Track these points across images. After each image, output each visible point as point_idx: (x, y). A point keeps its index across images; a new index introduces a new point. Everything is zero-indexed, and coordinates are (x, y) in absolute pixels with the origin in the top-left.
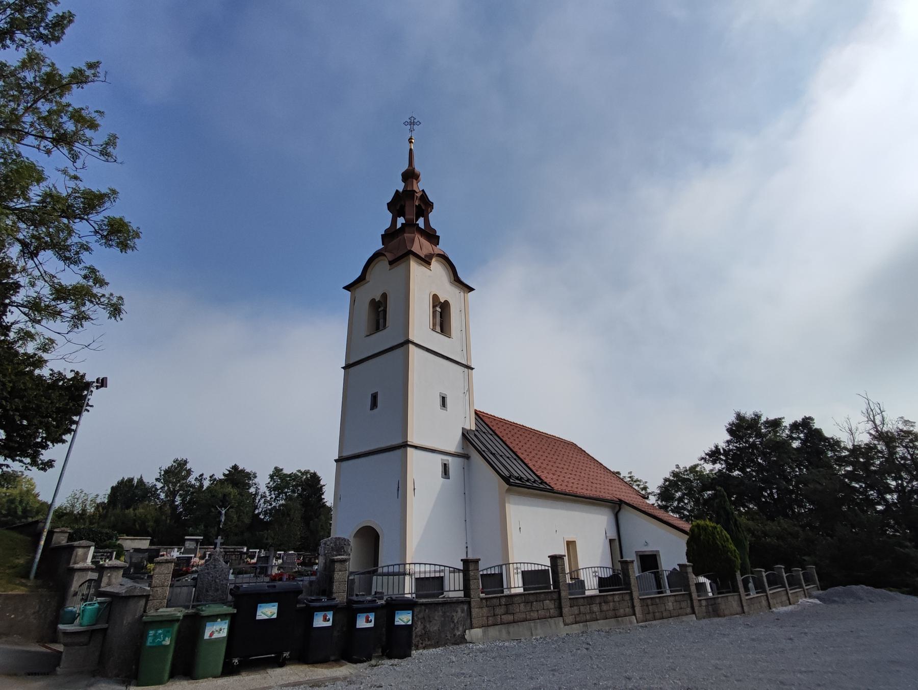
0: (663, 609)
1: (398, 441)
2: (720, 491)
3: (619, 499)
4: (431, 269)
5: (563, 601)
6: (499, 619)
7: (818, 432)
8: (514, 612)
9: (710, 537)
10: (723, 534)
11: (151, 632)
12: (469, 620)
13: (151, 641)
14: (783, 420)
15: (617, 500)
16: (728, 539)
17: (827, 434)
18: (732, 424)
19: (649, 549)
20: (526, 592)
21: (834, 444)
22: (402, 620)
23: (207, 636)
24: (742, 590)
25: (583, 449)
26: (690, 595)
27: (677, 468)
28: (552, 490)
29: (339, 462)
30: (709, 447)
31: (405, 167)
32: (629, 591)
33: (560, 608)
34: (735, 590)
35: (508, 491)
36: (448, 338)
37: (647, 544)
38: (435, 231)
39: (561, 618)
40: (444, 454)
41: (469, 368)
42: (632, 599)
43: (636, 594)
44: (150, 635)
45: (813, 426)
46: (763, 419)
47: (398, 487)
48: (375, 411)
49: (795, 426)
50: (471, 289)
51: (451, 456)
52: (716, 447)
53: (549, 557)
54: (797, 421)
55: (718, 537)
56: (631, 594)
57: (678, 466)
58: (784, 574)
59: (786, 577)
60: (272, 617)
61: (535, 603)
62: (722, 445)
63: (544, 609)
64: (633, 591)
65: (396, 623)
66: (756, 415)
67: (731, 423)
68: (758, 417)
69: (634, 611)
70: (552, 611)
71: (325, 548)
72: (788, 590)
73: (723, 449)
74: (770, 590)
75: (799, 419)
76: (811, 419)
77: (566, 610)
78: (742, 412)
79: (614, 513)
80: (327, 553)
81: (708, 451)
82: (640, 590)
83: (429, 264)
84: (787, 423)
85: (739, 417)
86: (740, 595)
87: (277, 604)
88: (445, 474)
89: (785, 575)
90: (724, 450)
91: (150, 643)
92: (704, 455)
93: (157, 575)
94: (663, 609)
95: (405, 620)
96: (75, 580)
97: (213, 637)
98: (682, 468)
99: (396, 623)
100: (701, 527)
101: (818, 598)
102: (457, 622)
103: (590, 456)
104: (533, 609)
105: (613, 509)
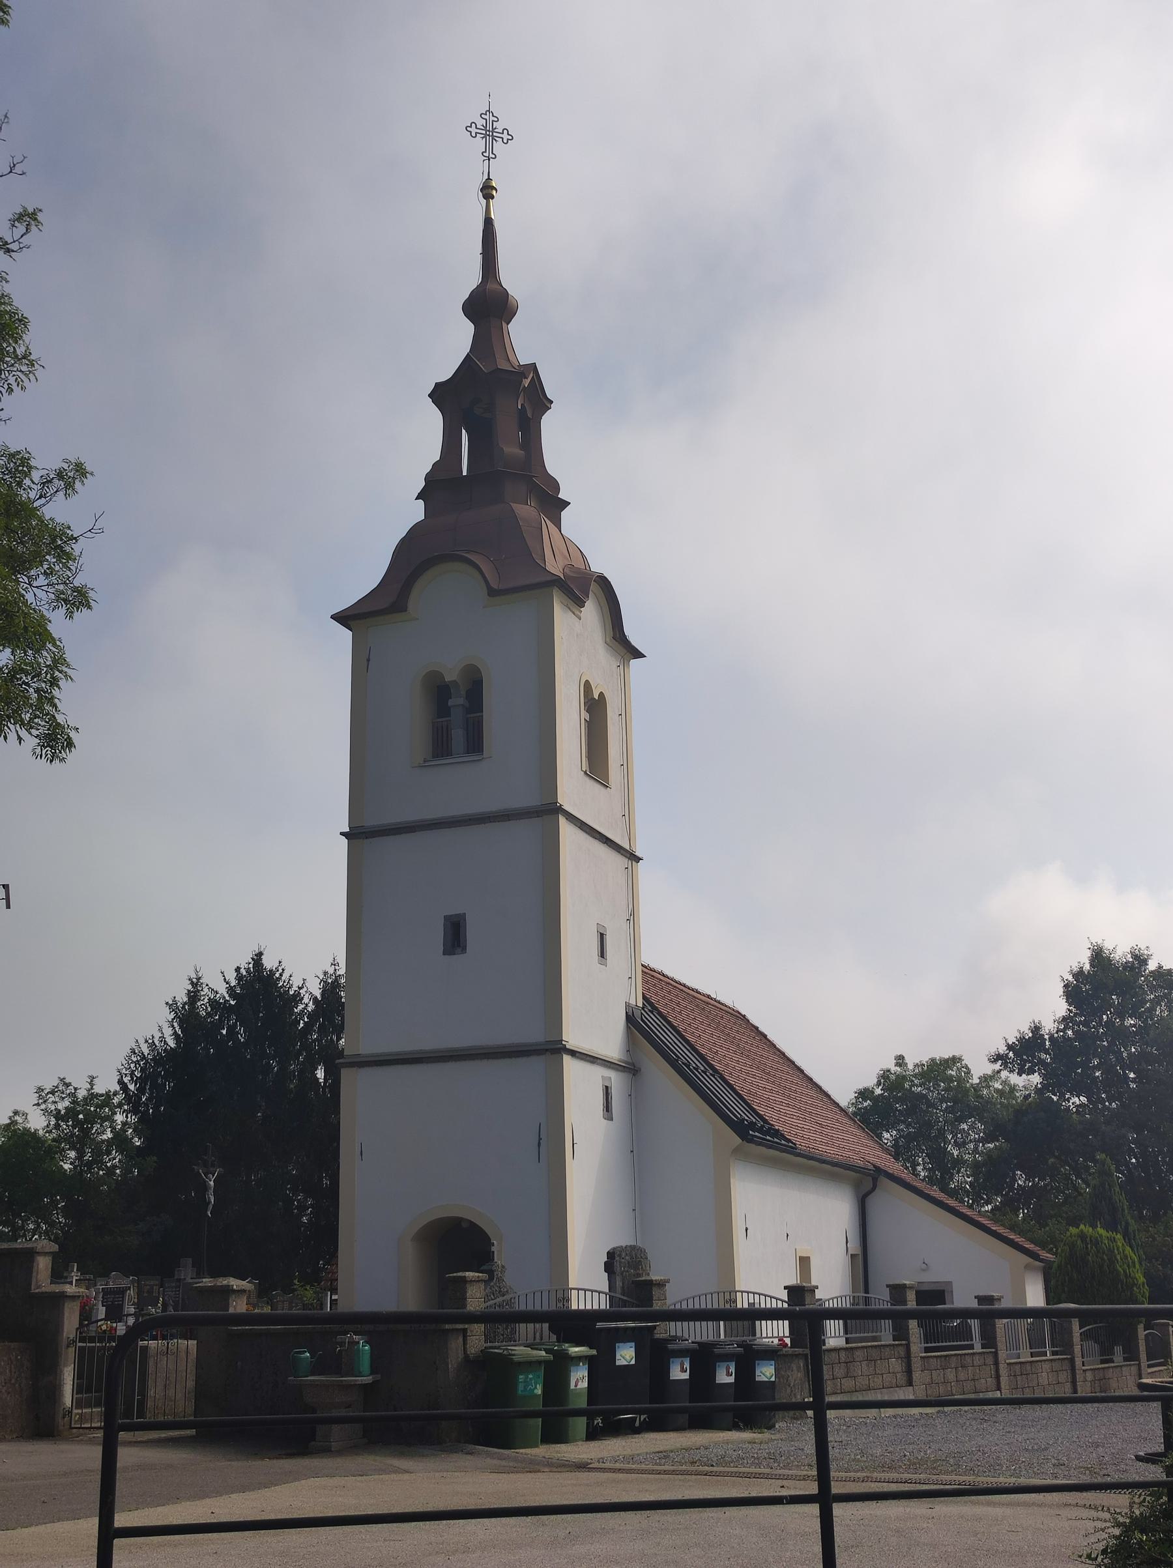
0: (1035, 1383)
1: (534, 1035)
2: (1103, 1163)
3: (874, 1166)
4: (582, 615)
5: (913, 1360)
6: (839, 1384)
8: (855, 1375)
9: (1105, 1257)
10: (1127, 1252)
11: (521, 1377)
12: (807, 1383)
13: (522, 1389)
15: (871, 1167)
16: (1134, 1262)
18: (1079, 975)
20: (848, 1345)
22: (764, 1375)
23: (572, 1386)
25: (762, 1029)
26: (1072, 1361)
27: (898, 1064)
28: (791, 1149)
30: (1015, 1027)
31: (472, 278)
32: (993, 1350)
33: (909, 1371)
35: (736, 1151)
36: (602, 789)
37: (926, 1267)
38: (556, 486)
39: (911, 1387)
40: (588, 1061)
41: (634, 858)
42: (996, 1363)
43: (1002, 1355)
44: (520, 1380)
46: (1152, 966)
47: (540, 1139)
48: (456, 959)
50: (638, 654)
51: (613, 1068)
52: (1036, 1029)
53: (785, 1288)
55: (1118, 1257)
56: (996, 1354)
60: (631, 1363)
61: (879, 1362)
62: (1049, 1026)
63: (889, 1373)
64: (999, 1349)
67: (1076, 969)
68: (1140, 960)
70: (899, 1376)
71: (620, 1262)
73: (1051, 1038)
74: (1149, 1366)
77: (916, 1376)
78: (1108, 945)
80: (624, 1271)
81: (1014, 1040)
82: (1008, 1349)
83: (581, 604)
85: (1099, 957)
86: (1139, 1365)
87: (633, 1344)
88: (607, 1111)
90: (1051, 1038)
91: (522, 1391)
92: (1003, 1049)
93: (470, 1300)
94: (1035, 1383)
95: (768, 1374)
96: (65, 1317)
97: (578, 1387)
98: (910, 1067)
100: (1088, 1239)
102: (794, 1386)
104: (878, 1372)
105: (857, 1186)
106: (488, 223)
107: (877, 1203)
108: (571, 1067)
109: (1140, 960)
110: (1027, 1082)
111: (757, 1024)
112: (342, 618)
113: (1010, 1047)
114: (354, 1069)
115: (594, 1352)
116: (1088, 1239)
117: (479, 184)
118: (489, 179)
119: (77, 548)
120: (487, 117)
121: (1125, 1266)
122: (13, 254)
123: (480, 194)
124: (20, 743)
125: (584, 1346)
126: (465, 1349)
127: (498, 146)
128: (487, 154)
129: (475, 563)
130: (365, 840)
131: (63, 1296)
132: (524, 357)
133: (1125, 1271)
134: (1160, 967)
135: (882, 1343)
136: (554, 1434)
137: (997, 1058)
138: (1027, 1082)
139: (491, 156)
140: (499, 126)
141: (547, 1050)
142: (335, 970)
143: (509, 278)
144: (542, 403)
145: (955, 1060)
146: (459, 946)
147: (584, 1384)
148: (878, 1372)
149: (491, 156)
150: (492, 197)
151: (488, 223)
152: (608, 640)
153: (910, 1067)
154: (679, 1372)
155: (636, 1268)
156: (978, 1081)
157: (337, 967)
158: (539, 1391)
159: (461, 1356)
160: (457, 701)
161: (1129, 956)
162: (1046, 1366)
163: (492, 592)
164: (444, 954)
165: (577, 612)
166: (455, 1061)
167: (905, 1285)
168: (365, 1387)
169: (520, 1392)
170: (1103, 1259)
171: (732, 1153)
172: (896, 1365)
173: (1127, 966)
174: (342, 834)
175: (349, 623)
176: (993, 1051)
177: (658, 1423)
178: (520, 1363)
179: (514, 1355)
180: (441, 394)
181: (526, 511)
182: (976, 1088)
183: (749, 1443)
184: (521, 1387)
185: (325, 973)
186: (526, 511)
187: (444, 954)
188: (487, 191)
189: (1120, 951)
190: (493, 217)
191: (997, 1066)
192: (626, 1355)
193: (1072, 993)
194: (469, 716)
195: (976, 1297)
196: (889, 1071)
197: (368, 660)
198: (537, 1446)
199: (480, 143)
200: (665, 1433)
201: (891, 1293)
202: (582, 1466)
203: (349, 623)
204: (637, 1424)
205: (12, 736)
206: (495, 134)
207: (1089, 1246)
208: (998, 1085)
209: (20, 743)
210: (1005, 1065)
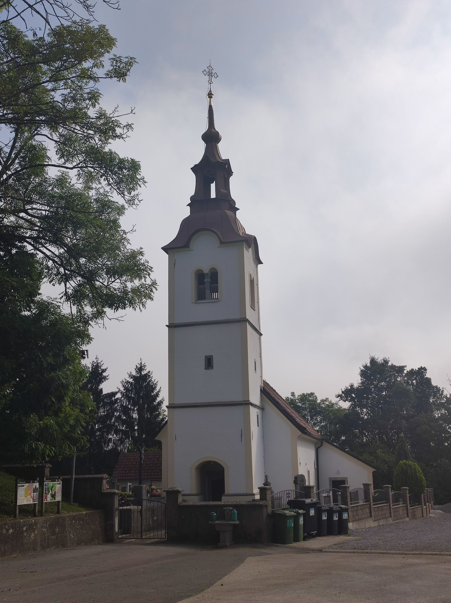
7: (429, 380)
14: (405, 368)
17: (434, 383)
19: (342, 475)
21: (437, 391)
24: (423, 504)
26: (407, 506)
29: (169, 408)
30: (344, 385)
31: (204, 128)
33: (371, 512)
34: (420, 504)
35: (299, 438)
36: (253, 310)
37: (338, 473)
38: (234, 203)
41: (261, 335)
42: (390, 508)
45: (425, 375)
46: (390, 364)
47: (242, 434)
48: (209, 371)
49: (412, 372)
54: (413, 369)
57: (293, 394)
58: (408, 494)
59: (409, 496)
62: (356, 385)
65: (343, 518)
66: (384, 361)
67: (364, 365)
69: (391, 515)
70: (368, 514)
72: (372, 505)
74: (374, 505)
75: (416, 368)
76: (425, 369)
77: (373, 514)
78: (376, 357)
79: (315, 448)
84: (408, 369)
89: (408, 495)
92: (341, 393)
98: (296, 396)
99: (343, 518)
100: (407, 465)
101: (440, 509)
103: (279, 395)
105: (316, 444)
106: (210, 108)
107: (321, 450)
108: (252, 409)
109: (386, 362)
110: (346, 405)
111: (272, 387)
112: (165, 249)
113: (343, 392)
114: (173, 409)
115: (305, 512)
116: (407, 465)
117: (207, 92)
118: (210, 91)
119: (128, 236)
120: (209, 68)
121: (420, 474)
122: (124, 139)
123: (207, 96)
124: (141, 312)
125: (301, 510)
126: (267, 512)
127: (213, 79)
128: (209, 82)
129: (216, 232)
130: (175, 328)
131: (115, 493)
132: (224, 156)
133: (419, 476)
134: (392, 365)
135: (360, 504)
136: (296, 539)
137: (338, 396)
138: (346, 405)
139: (211, 82)
140: (214, 72)
141: (244, 404)
142: (97, 361)
143: (218, 127)
144: (230, 173)
145: (312, 394)
146: (210, 366)
147: (302, 523)
148: (364, 513)
149: (211, 82)
150: (212, 97)
151: (210, 108)
152: (254, 258)
153: (296, 396)
154: (324, 518)
155: (303, 482)
156: (320, 401)
157: (98, 360)
158: (293, 525)
159: (266, 514)
160: (207, 280)
161: (383, 361)
162: (401, 508)
163: (222, 243)
164: (205, 369)
165: (248, 250)
166: (210, 407)
167: (369, 484)
168: (235, 525)
169: (288, 526)
170: (413, 472)
171: (298, 437)
172: (367, 510)
173: (382, 365)
174: (166, 326)
175: (168, 250)
176: (337, 394)
177: (319, 534)
178: (288, 516)
179: (286, 514)
180: (195, 169)
181: (229, 213)
182: (319, 404)
183: (355, 540)
184: (288, 524)
185: (93, 362)
186: (229, 213)
187: (205, 369)
188: (210, 95)
189: (380, 360)
190: (212, 105)
191: (338, 399)
192: (312, 512)
193: (363, 374)
194: (211, 285)
195: (363, 484)
196: (288, 397)
197: (175, 264)
198: (292, 543)
199: (207, 78)
200: (320, 537)
201: (364, 487)
202: (320, 551)
203: (168, 250)
204: (314, 534)
205: (138, 309)
206: (212, 74)
207: (408, 467)
208: (327, 403)
209: (141, 312)
210: (341, 399)
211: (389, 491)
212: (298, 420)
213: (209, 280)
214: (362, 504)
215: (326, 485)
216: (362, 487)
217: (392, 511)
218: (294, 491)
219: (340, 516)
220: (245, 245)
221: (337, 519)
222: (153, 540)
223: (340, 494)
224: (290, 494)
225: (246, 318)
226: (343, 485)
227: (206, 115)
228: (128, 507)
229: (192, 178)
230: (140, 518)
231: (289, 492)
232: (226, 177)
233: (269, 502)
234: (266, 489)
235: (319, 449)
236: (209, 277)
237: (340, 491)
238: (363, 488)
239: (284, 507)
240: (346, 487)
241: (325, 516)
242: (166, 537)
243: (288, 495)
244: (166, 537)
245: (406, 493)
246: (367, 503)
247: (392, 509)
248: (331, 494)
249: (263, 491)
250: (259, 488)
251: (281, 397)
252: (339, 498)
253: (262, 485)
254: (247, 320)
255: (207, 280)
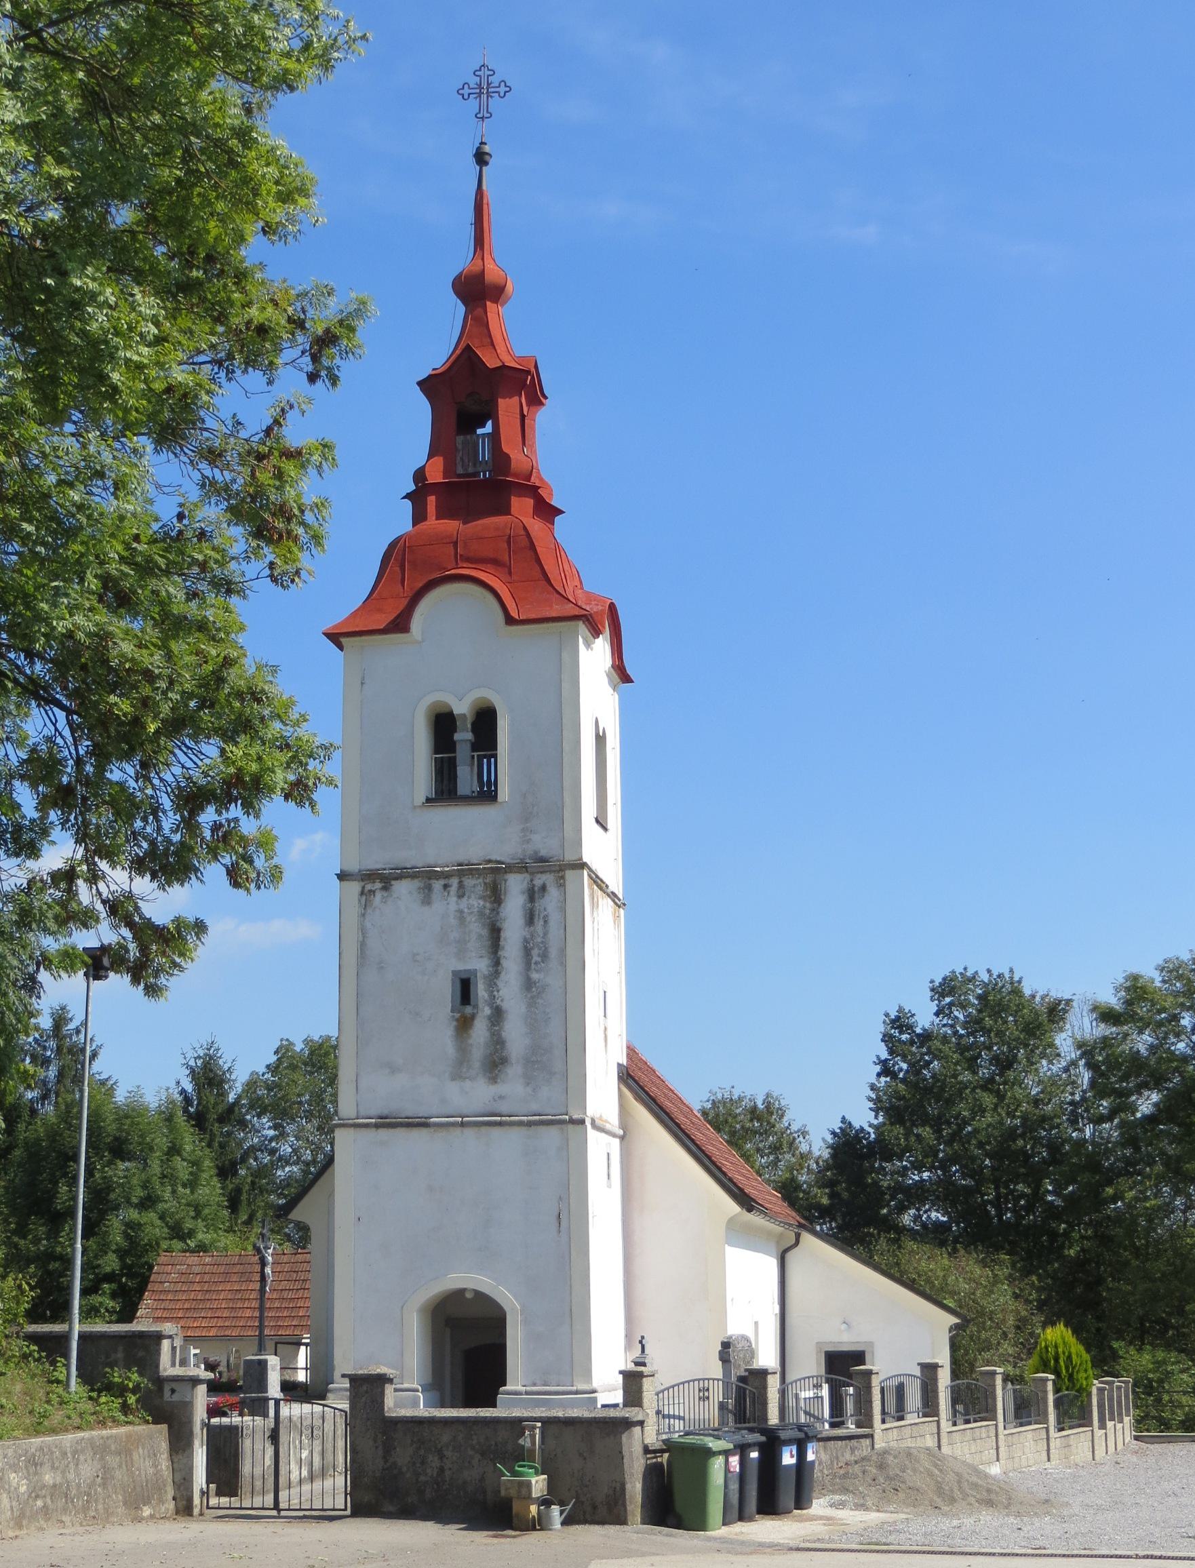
41: (400, 624)
150: (486, 163)
160: (463, 736)
180: (429, 386)
188: (481, 158)
195: (919, 1364)
211: (994, 1386)
212: (727, 1166)
213: (469, 736)
214: (913, 1422)
215: (808, 1364)
216: (917, 1371)
217: (1001, 1443)
218: (721, 1383)
219: (801, 1455)
220: (582, 628)
221: (793, 1461)
222: (301, 1514)
223: (851, 1392)
224: (708, 1390)
225: (581, 859)
226: (861, 1367)
227: (470, 215)
228: (225, 1420)
229: (420, 413)
230: (270, 1451)
231: (706, 1385)
232: (525, 413)
233: (648, 1411)
234: (640, 1375)
235: (790, 1256)
236: (469, 726)
237: (852, 1385)
238: (919, 1374)
239: (692, 1428)
240: (869, 1373)
241: (792, 1456)
242: (349, 1505)
243: (701, 1394)
244: (349, 1505)
245: (1046, 1392)
246: (931, 1419)
247: (1001, 1437)
248: (825, 1391)
249: (633, 1381)
250: (621, 1372)
251: (673, 1091)
252: (849, 1406)
253: (631, 1367)
254: (583, 865)
255: (463, 736)
